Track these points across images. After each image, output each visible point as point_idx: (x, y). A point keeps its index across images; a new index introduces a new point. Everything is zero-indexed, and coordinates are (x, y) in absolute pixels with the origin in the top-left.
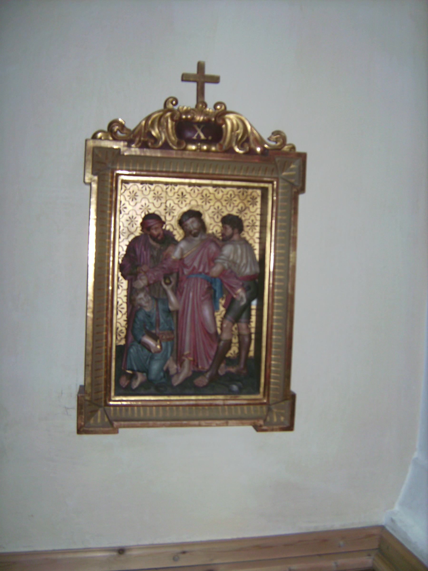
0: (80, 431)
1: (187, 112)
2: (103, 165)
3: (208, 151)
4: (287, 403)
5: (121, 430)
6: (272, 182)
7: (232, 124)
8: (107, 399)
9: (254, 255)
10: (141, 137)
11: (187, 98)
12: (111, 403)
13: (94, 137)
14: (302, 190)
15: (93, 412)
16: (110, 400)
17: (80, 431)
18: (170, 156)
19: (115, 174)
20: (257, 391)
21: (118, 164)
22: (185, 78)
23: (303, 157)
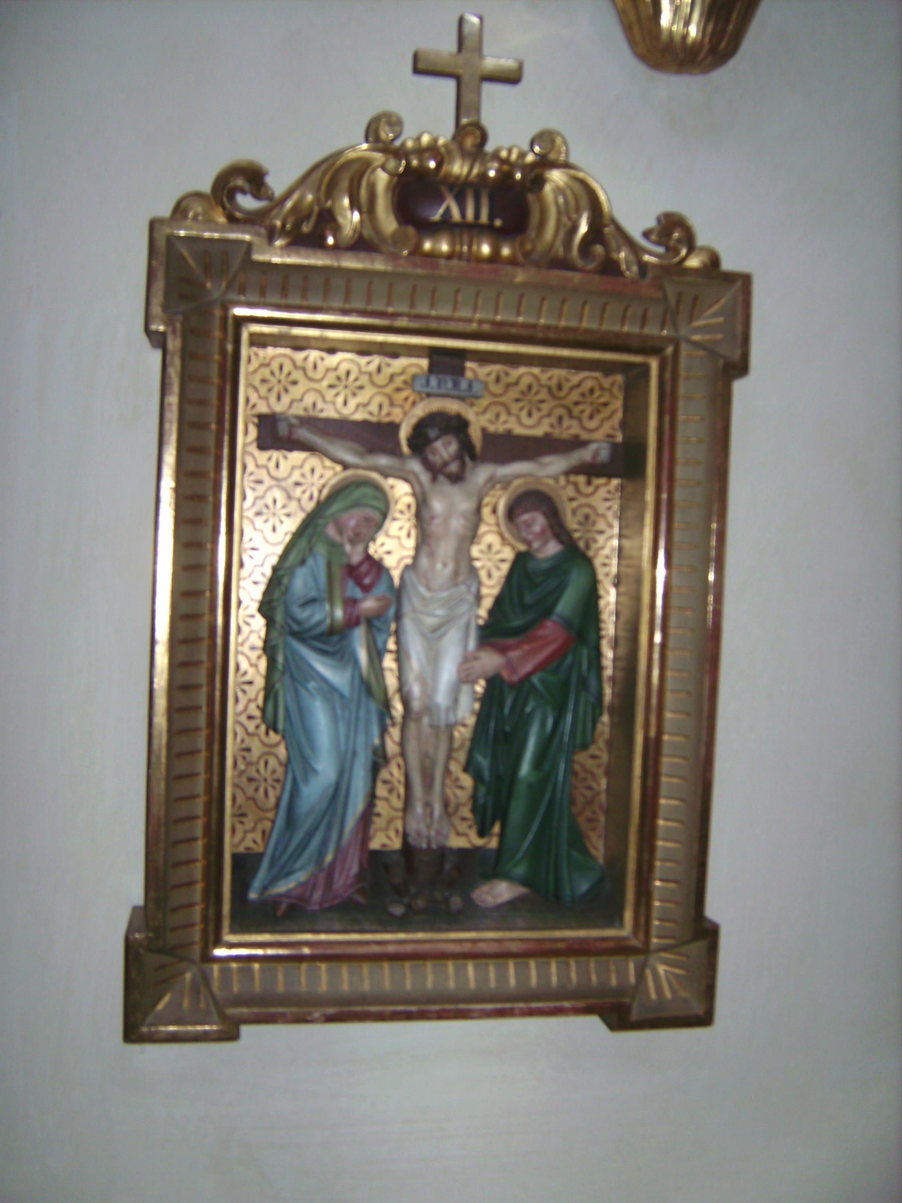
0: (132, 1033)
1: (432, 150)
2: (196, 293)
3: (495, 257)
4: (697, 948)
5: (245, 1029)
9: (705, 618)
11: (428, 116)
12: (220, 952)
13: (180, 210)
14: (741, 368)
16: (218, 942)
17: (132, 1033)
19: (230, 322)
21: (690, 40)
22: (422, 67)
23: (744, 281)
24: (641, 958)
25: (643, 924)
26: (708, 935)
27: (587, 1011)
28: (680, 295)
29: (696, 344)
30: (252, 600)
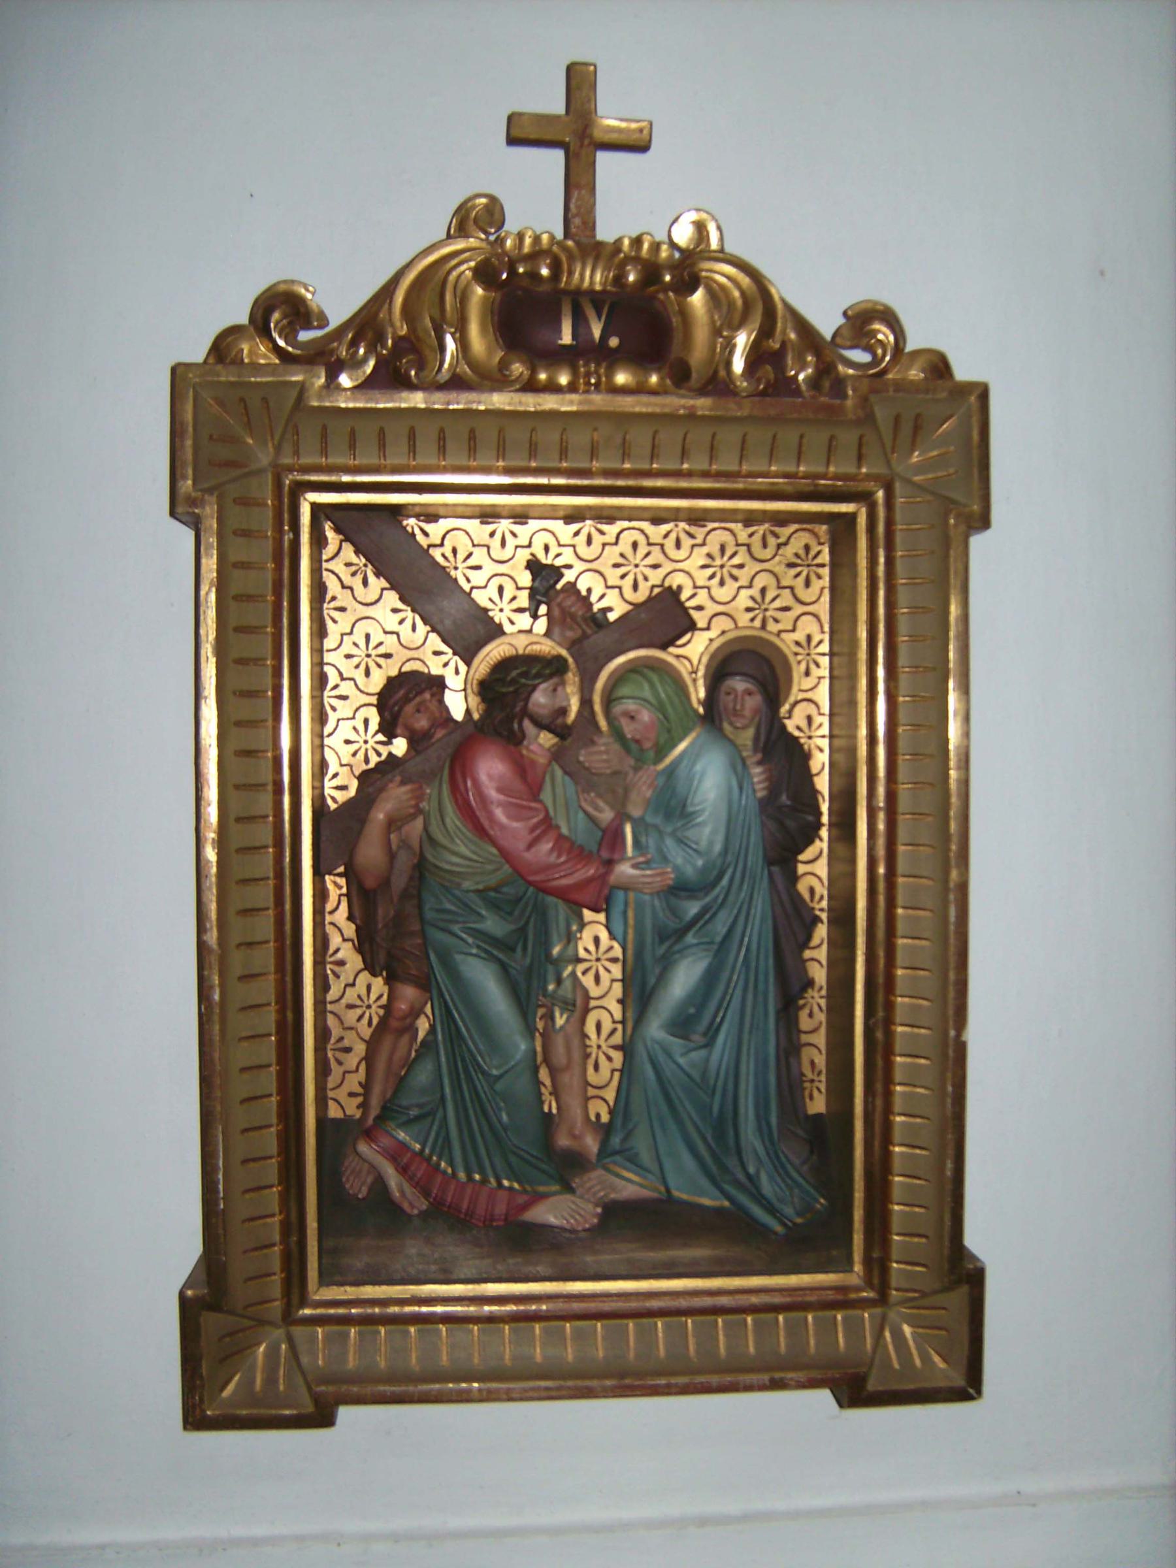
4: (958, 1298)
6: (865, 497)
7: (743, 293)
8: (295, 1299)
10: (395, 336)
11: (533, 200)
15: (252, 1346)
16: (304, 1302)
18: (469, 245)
20: (848, 1267)
22: (523, 133)
23: (982, 393)
24: (878, 1311)
25: (877, 1268)
26: (966, 1277)
27: (812, 1384)
28: (897, 420)
29: (918, 486)
30: (386, 632)
